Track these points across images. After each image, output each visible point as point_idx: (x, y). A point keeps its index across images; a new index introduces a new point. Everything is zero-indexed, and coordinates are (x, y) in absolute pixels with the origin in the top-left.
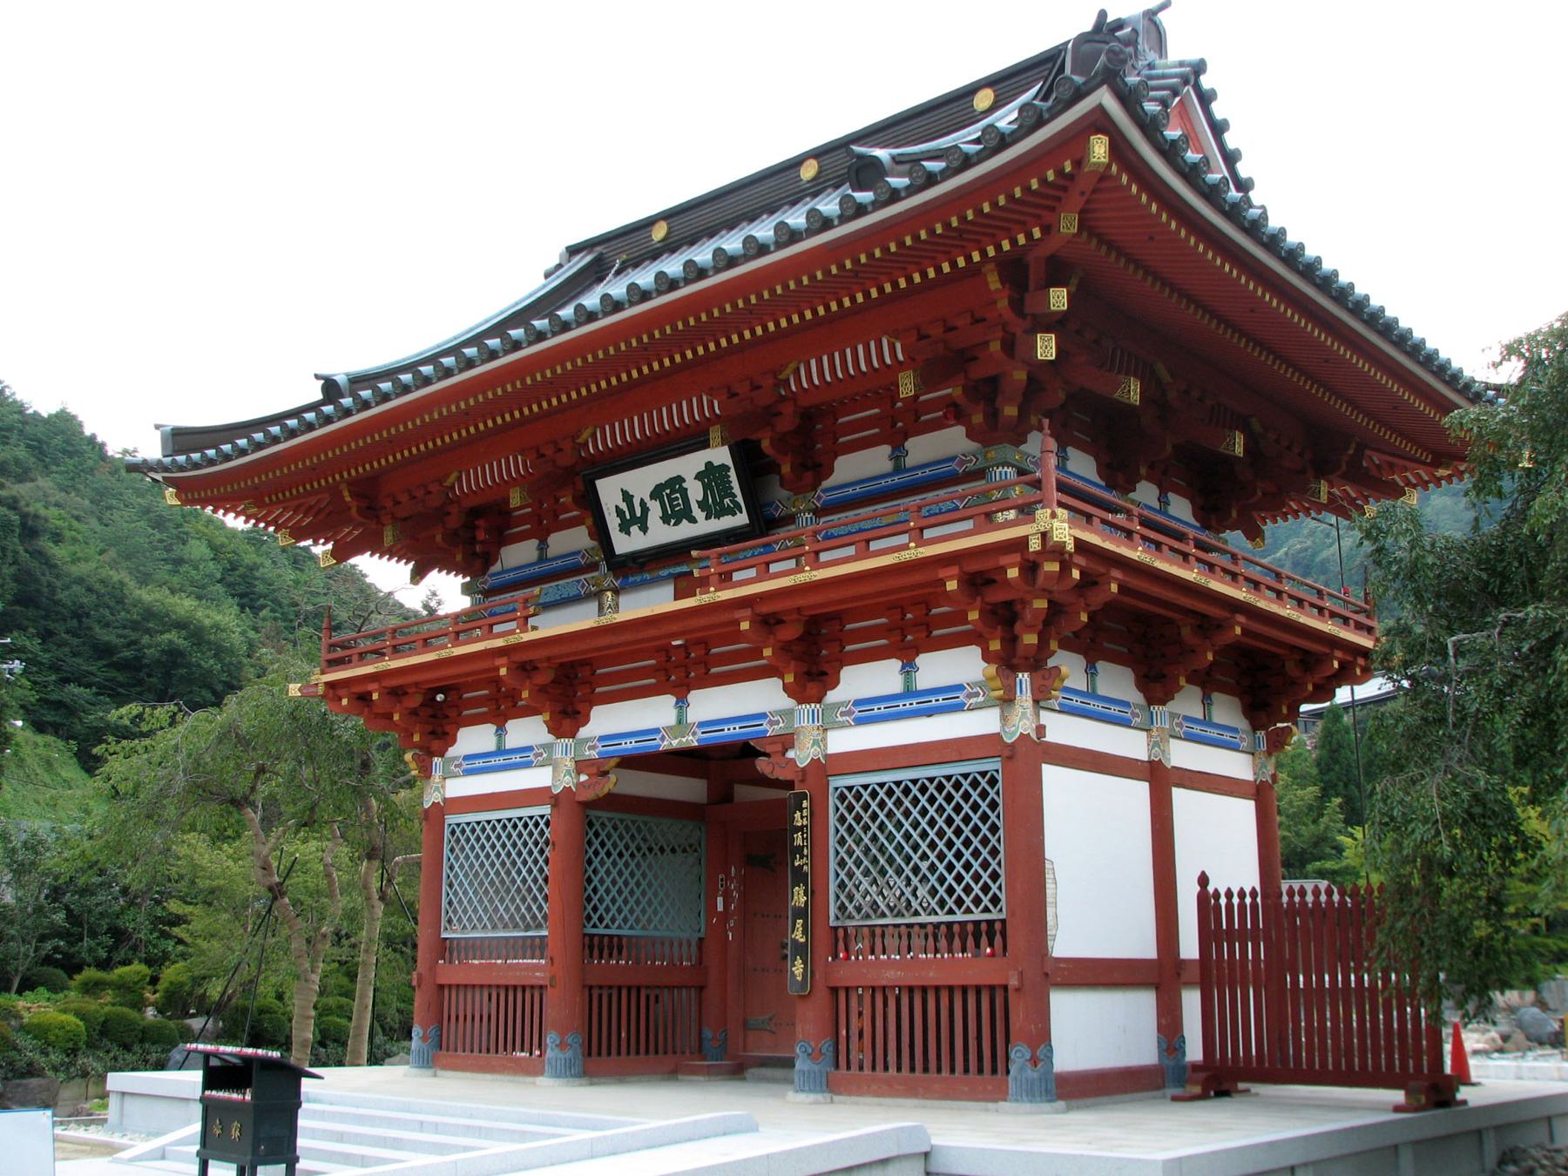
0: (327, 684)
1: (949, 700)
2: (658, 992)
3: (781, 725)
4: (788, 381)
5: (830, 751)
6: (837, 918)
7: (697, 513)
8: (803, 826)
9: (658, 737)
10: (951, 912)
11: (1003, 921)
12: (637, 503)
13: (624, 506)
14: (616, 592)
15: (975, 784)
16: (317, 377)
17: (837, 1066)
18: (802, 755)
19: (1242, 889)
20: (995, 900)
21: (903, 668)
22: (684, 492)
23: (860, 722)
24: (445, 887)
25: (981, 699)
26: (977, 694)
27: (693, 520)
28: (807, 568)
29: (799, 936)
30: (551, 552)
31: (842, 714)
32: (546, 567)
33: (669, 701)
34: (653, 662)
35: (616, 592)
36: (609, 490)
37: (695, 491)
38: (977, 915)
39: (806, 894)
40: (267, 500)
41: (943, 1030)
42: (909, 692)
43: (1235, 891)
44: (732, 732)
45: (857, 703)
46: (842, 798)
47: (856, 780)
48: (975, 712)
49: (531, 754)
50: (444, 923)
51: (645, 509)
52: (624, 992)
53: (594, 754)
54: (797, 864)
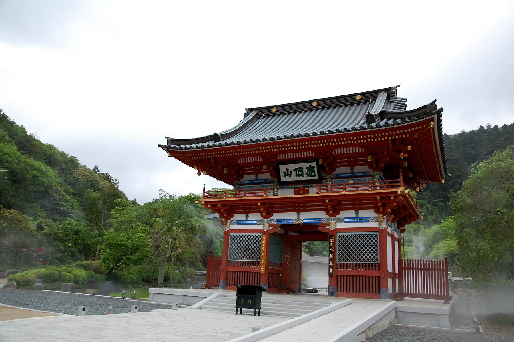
0: (205, 201)
1: (367, 220)
2: (272, 274)
3: (325, 221)
4: (238, 161)
6: (338, 261)
7: (305, 175)
11: (379, 264)
12: (289, 171)
13: (286, 171)
14: (278, 189)
15: (235, 237)
16: (166, 138)
17: (337, 291)
18: (332, 227)
19: (413, 260)
20: (376, 260)
21: (356, 212)
22: (302, 171)
23: (345, 222)
24: (229, 249)
25: (374, 220)
26: (373, 219)
31: (273, 222)
32: (257, 181)
33: (296, 213)
35: (278, 189)
36: (282, 168)
37: (305, 171)
39: (333, 256)
42: (247, 220)
43: (414, 260)
45: (344, 218)
46: (340, 237)
47: (343, 234)
48: (373, 223)
49: (256, 222)
50: (228, 258)
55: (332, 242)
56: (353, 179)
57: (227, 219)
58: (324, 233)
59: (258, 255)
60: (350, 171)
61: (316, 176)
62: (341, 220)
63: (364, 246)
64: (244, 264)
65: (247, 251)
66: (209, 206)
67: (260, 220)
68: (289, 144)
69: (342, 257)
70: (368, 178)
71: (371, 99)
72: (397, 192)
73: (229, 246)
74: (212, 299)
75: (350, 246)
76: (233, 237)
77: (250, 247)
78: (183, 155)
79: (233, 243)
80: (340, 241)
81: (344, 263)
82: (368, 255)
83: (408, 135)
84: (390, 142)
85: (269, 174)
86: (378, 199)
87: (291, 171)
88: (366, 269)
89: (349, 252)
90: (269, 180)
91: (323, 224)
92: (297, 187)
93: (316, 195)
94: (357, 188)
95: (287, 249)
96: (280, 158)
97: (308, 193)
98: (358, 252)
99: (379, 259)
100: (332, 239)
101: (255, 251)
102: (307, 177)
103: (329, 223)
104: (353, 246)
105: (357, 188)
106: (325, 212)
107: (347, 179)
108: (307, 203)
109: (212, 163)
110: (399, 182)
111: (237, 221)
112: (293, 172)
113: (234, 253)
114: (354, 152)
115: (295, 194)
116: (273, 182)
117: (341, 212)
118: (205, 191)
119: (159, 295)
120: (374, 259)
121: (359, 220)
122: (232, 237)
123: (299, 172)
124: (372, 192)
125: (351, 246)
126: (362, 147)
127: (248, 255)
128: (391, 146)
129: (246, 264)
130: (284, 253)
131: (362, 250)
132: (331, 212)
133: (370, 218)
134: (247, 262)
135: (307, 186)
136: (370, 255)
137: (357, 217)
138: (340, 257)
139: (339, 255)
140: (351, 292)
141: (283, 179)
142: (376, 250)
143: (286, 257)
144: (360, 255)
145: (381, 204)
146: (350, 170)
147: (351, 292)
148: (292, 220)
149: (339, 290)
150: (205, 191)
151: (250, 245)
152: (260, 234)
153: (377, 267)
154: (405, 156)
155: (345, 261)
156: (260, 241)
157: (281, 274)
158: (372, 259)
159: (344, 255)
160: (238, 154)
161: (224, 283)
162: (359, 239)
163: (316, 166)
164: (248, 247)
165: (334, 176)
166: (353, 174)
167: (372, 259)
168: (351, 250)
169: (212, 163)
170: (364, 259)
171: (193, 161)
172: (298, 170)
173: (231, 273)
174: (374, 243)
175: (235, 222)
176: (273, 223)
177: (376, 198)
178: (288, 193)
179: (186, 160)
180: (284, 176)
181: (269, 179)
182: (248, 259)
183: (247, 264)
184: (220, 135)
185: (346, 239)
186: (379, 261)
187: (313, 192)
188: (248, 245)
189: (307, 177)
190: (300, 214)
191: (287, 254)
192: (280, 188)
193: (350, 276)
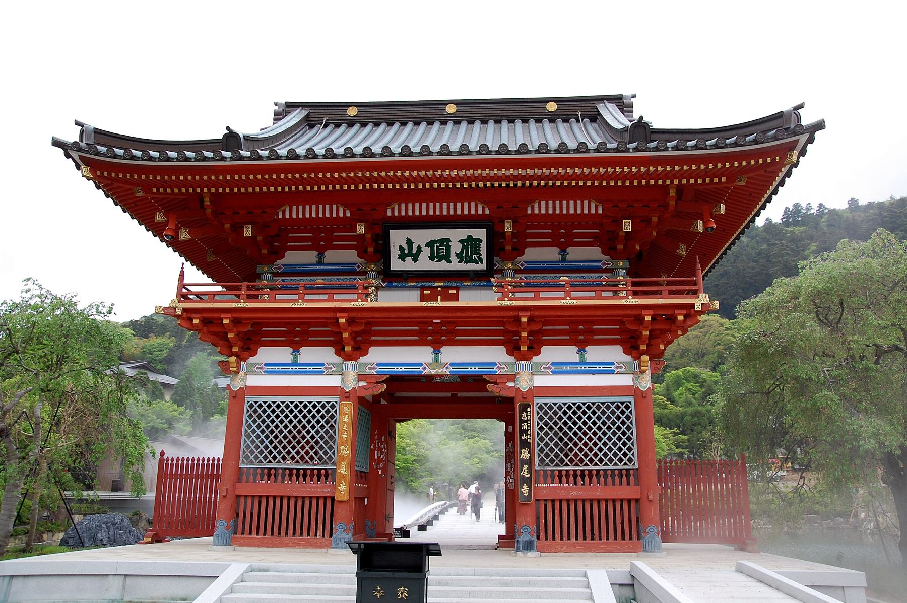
1: (606, 368)
5: (534, 386)
6: (539, 465)
7: (453, 257)
9: (421, 368)
10: (606, 464)
13: (406, 247)
15: (260, 406)
16: (77, 123)
17: (538, 538)
18: (524, 385)
20: (630, 460)
22: (449, 248)
23: (554, 373)
24: (243, 437)
25: (623, 369)
26: (622, 367)
27: (450, 262)
28: (630, 297)
29: (525, 473)
30: (326, 260)
33: (429, 349)
34: (417, 328)
36: (398, 237)
37: (456, 248)
39: (529, 453)
40: (154, 190)
41: (556, 517)
43: (216, 459)
44: (471, 370)
46: (541, 408)
49: (495, 367)
50: (240, 462)
51: (419, 249)
54: (523, 438)
55: (527, 421)
56: (322, 278)
57: (241, 358)
59: (326, 453)
60: (558, 258)
62: (544, 368)
63: (599, 428)
64: (287, 477)
65: (294, 443)
66: (196, 322)
67: (333, 364)
69: (547, 456)
70: (357, 277)
72: (692, 306)
73: (243, 430)
74: (244, 573)
75: (565, 429)
76: (256, 406)
77: (304, 432)
79: (255, 421)
80: (541, 418)
81: (553, 471)
82: (610, 450)
83: (724, 180)
84: (673, 193)
85: (354, 253)
86: (342, 321)
87: (419, 246)
88: (606, 484)
89: (566, 445)
90: (355, 267)
91: (500, 376)
93: (500, 303)
95: (380, 439)
97: (457, 300)
98: (586, 444)
99: (636, 459)
100: (527, 412)
101: (317, 443)
103: (515, 375)
104: (575, 429)
109: (208, 211)
110: (695, 283)
111: (266, 364)
113: (257, 447)
114: (314, 215)
115: (422, 300)
116: (364, 273)
117: (544, 349)
118: (185, 282)
119: (32, 582)
120: (625, 460)
121: (298, 368)
122: (251, 406)
123: (440, 250)
124: (637, 303)
125: (570, 428)
126: (346, 205)
127: (298, 453)
128: (672, 203)
129: (291, 475)
130: (372, 447)
131: (595, 439)
132: (348, 349)
133: (325, 365)
135: (454, 284)
136: (615, 449)
137: (582, 362)
138: (542, 455)
139: (542, 450)
140: (573, 539)
141: (396, 265)
142: (629, 439)
143: (376, 458)
144: (591, 450)
147: (573, 539)
148: (421, 364)
149: (542, 535)
150: (185, 282)
151: (304, 427)
152: (333, 399)
153: (624, 477)
154: (711, 226)
155: (557, 465)
156: (332, 417)
157: (366, 500)
158: (621, 460)
159: (552, 450)
161: (227, 530)
162: (589, 413)
163: (484, 238)
164: (299, 432)
165: (522, 265)
166: (564, 265)
167: (621, 460)
168: (571, 439)
169: (208, 211)
170: (601, 461)
171: (153, 198)
172: (438, 245)
173: (249, 500)
174: (623, 423)
175: (262, 368)
176: (368, 371)
179: (133, 194)
180: (399, 258)
181: (355, 264)
182: (297, 462)
183: (294, 477)
184: (241, 136)
185: (555, 413)
186: (637, 464)
188: (299, 427)
189: (458, 263)
191: (378, 451)
192: (383, 288)
193: (568, 500)
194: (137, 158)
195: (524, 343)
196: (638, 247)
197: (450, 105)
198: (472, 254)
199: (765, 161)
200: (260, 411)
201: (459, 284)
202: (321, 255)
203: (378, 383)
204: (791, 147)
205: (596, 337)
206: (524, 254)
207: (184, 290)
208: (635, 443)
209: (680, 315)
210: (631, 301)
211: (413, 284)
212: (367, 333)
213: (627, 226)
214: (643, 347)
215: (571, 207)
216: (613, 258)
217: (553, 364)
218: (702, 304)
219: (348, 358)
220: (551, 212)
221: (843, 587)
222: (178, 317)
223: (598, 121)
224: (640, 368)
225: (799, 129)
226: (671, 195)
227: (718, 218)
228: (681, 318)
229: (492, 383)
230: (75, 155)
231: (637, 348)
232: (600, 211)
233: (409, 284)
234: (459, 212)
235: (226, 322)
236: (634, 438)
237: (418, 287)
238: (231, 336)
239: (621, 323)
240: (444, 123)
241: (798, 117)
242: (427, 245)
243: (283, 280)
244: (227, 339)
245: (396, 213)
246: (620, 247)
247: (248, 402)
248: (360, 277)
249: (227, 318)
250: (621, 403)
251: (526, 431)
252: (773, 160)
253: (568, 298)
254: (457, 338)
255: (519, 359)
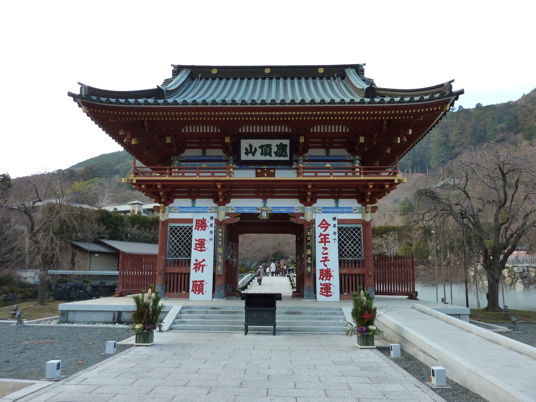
1: (349, 210)
3: (299, 210)
7: (273, 154)
8: (310, 235)
10: (348, 257)
13: (249, 148)
16: (79, 83)
20: (360, 255)
22: (270, 149)
23: (323, 212)
24: (168, 245)
25: (357, 211)
27: (271, 156)
28: (363, 176)
29: (309, 261)
31: (231, 210)
33: (261, 200)
36: (245, 144)
37: (274, 149)
38: (355, 258)
39: (311, 251)
40: (119, 118)
44: (284, 211)
48: (355, 214)
49: (294, 209)
50: (167, 256)
52: (347, 277)
53: (233, 211)
55: (310, 236)
57: (166, 204)
58: (296, 225)
61: (287, 157)
67: (213, 207)
68: (406, 112)
71: (200, 75)
72: (393, 180)
73: (168, 241)
78: (106, 112)
83: (412, 117)
84: (385, 123)
86: (219, 186)
92: (259, 169)
94: (316, 173)
96: (242, 130)
97: (274, 176)
99: (363, 255)
100: (310, 231)
102: (275, 156)
105: (316, 173)
106: (357, 200)
107: (323, 163)
108: (274, 187)
112: (258, 149)
115: (257, 176)
117: (318, 200)
120: (358, 255)
122: (171, 228)
123: (266, 149)
128: (385, 128)
132: (221, 200)
134: (183, 261)
135: (273, 167)
141: (244, 157)
142: (360, 245)
145: (222, 193)
146: (202, 152)
158: (355, 255)
160: (216, 119)
163: (288, 144)
165: (307, 158)
167: (355, 255)
172: (265, 147)
177: (216, 186)
178: (249, 175)
186: (363, 257)
187: (282, 175)
189: (275, 156)
190: (266, 201)
194: (113, 103)
195: (309, 198)
196: (366, 149)
197: (267, 69)
198: (282, 152)
199: (433, 109)
200: (176, 231)
201: (275, 167)
202: (204, 152)
203: (236, 217)
204: (446, 102)
205: (344, 195)
206: (308, 152)
207: (136, 170)
208: (362, 247)
209: (387, 185)
210: (363, 178)
211: (252, 167)
212: (230, 192)
213: (362, 140)
214: (368, 200)
215: (333, 129)
216: (353, 155)
217: (322, 208)
218: (398, 180)
219: (221, 204)
220: (322, 131)
221: (459, 315)
222: (134, 184)
223: (345, 79)
224: (366, 210)
225: (452, 94)
226: (384, 124)
227: (408, 136)
228: (387, 186)
229: (292, 217)
230: (79, 100)
231: (364, 200)
232: (348, 131)
233: (250, 167)
234: (276, 131)
235: (159, 187)
236: (362, 244)
237: (254, 168)
238: (161, 193)
239: (357, 188)
240: (264, 79)
241: (451, 87)
242: (260, 147)
243: (185, 165)
244: (159, 195)
245: (244, 131)
246: (357, 149)
247: (170, 226)
248: (225, 163)
249: (159, 185)
250: (356, 227)
251: (309, 241)
252: (437, 109)
253: (332, 176)
254: (275, 194)
255: (305, 205)
